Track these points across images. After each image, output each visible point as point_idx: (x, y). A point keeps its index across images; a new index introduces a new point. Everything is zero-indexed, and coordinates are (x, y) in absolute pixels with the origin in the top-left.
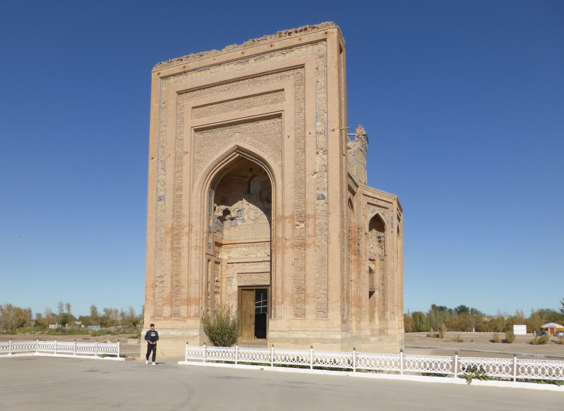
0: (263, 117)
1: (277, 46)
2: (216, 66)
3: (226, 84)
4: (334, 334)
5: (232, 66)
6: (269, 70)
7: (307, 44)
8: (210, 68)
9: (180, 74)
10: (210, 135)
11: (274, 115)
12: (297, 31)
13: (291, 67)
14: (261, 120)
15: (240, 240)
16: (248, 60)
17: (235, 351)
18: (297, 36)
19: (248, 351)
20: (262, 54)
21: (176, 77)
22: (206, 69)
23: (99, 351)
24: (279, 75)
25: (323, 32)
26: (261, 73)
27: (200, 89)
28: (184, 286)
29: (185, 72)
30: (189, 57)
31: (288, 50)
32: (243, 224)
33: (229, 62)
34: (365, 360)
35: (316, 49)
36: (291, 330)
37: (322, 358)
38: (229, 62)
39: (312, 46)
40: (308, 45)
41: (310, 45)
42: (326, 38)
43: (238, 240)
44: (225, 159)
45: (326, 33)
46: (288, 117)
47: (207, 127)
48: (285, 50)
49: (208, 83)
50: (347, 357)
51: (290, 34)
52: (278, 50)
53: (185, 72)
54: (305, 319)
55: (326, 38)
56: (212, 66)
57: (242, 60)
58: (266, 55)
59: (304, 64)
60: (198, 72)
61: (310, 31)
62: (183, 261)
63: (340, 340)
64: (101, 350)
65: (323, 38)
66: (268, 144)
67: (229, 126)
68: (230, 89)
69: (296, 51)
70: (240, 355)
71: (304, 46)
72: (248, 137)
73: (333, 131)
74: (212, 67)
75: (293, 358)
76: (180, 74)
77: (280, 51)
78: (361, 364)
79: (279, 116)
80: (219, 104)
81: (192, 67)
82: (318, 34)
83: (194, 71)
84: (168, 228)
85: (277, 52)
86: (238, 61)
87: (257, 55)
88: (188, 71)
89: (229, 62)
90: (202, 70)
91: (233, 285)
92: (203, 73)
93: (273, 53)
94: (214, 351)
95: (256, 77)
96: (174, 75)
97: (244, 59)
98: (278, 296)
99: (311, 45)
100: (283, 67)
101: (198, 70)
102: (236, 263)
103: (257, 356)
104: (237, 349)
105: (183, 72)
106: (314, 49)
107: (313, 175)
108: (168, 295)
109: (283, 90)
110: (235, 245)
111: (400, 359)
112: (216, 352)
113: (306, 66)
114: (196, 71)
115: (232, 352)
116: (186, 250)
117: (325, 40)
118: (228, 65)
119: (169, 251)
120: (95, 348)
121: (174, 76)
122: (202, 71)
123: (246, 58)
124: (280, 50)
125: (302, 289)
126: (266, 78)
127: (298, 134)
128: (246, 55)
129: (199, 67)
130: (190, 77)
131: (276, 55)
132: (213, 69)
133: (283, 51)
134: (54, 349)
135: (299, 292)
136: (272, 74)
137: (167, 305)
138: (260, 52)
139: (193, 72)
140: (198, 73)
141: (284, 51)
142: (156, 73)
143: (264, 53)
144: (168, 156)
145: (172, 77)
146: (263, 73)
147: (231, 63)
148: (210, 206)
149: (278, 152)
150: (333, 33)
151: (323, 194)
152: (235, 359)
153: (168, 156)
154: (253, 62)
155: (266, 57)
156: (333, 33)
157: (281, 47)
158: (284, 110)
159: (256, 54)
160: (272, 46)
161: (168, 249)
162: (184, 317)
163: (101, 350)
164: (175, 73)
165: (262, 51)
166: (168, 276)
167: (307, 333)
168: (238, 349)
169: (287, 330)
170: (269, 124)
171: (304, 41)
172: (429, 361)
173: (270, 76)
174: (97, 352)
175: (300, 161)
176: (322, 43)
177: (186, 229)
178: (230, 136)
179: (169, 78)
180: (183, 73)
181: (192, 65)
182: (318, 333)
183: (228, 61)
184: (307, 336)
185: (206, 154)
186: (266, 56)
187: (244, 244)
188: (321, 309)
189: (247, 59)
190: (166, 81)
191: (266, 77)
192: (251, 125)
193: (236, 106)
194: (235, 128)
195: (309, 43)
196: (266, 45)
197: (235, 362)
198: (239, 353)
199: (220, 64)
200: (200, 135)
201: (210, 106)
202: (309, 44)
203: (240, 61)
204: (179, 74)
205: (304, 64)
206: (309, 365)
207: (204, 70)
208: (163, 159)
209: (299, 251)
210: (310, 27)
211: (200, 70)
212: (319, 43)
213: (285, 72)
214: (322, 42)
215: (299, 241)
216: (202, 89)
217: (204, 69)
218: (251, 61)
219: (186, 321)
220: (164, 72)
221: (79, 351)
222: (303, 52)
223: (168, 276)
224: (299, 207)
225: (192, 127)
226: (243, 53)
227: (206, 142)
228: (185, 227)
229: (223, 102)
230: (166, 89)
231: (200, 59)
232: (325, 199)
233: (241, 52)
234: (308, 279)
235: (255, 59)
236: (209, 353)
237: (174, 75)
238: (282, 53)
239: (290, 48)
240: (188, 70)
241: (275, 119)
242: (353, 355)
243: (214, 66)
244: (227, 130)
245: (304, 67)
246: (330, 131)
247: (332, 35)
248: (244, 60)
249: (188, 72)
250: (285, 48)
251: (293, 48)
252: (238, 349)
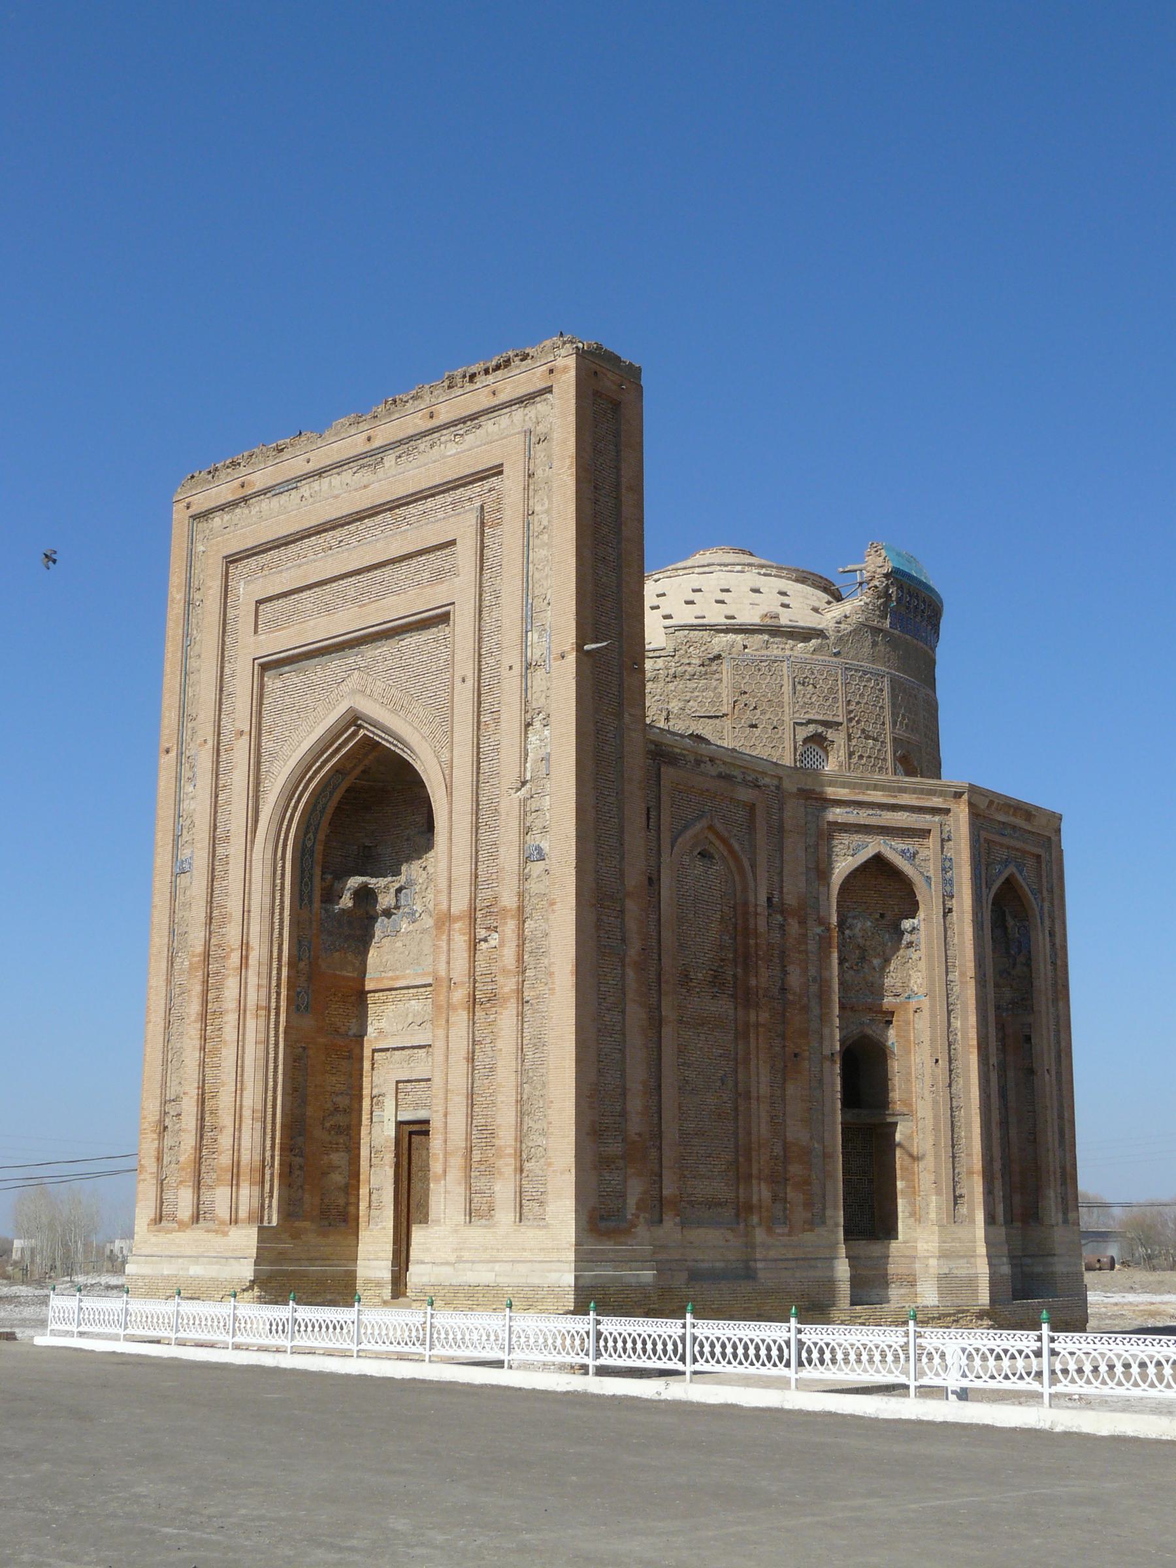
0: (410, 624)
1: (445, 414)
2: (312, 479)
3: (333, 528)
4: (559, 1271)
5: (347, 476)
6: (424, 487)
7: (511, 406)
8: (299, 484)
9: (233, 505)
10: (296, 680)
11: (351, 640)
12: (488, 368)
13: (472, 475)
14: (407, 631)
15: (404, 977)
16: (382, 459)
17: (684, 1334)
18: (488, 383)
19: (732, 1331)
20: (411, 438)
21: (228, 512)
22: (290, 487)
23: (606, 1350)
24: (448, 498)
25: (544, 368)
26: (407, 496)
27: (278, 547)
28: (224, 1127)
29: (245, 499)
30: (254, 456)
31: (469, 423)
32: (411, 928)
33: (341, 466)
34: (1159, 1364)
35: (530, 418)
36: (460, 1260)
37: (1097, 1360)
38: (339, 466)
39: (522, 409)
40: (514, 408)
41: (518, 406)
42: (552, 386)
43: (397, 978)
44: (331, 746)
45: (551, 371)
46: (463, 619)
47: (288, 658)
48: (462, 425)
49: (292, 531)
50: (1170, 1358)
51: (472, 377)
52: (446, 426)
53: (245, 499)
54: (493, 1226)
55: (552, 386)
56: (305, 479)
57: (368, 459)
58: (419, 441)
59: (502, 464)
60: (273, 496)
61: (517, 367)
62: (224, 1052)
63: (569, 1289)
64: (655, 1353)
65: (543, 385)
66: (423, 700)
67: (337, 651)
68: (342, 544)
69: (489, 427)
70: (804, 1355)
71: (505, 411)
72: (378, 683)
73: (563, 657)
74: (303, 482)
75: (1076, 1367)
76: (233, 505)
77: (452, 429)
78: (1114, 1378)
79: (444, 618)
80: (316, 589)
81: (259, 486)
82: (534, 374)
83: (265, 494)
84: (194, 956)
85: (445, 432)
86: (361, 462)
87: (400, 442)
88: (250, 495)
89: (339, 466)
90: (282, 490)
91: (386, 1120)
92: (284, 498)
93: (436, 435)
94: (991, 1351)
95: (398, 507)
96: (221, 508)
97: (371, 458)
98: (435, 1154)
99: (520, 407)
100: (456, 477)
101: (273, 493)
102: (394, 1049)
103: (1148, 1371)
104: (1045, 1339)
105: (241, 498)
106: (527, 418)
107: (520, 789)
108: (189, 1156)
109: (452, 543)
110: (393, 992)
111: (1041, 1348)
112: (974, 1353)
113: (506, 469)
114: (269, 495)
115: (895, 1346)
116: (231, 1018)
117: (549, 390)
118: (338, 474)
119: (195, 1022)
120: (788, 1346)
121: (223, 510)
122: (282, 493)
123: (377, 452)
124: (453, 426)
125: (490, 1132)
126: (421, 508)
127: (489, 669)
128: (376, 443)
129: (274, 483)
130: (257, 512)
131: (443, 439)
132: (305, 489)
133: (459, 427)
134: (588, 1350)
135: (483, 1140)
136: (433, 495)
137: (185, 1186)
138: (406, 436)
139: (262, 497)
140: (275, 499)
141: (460, 428)
142: (184, 504)
143: (418, 437)
144: (200, 745)
145: (218, 513)
146: (412, 495)
147: (346, 467)
148: (306, 884)
149: (443, 724)
150: (565, 369)
151: (541, 845)
152: (684, 1363)
153: (200, 745)
154: (394, 462)
155: (422, 447)
156: (565, 369)
157: (453, 416)
158: (454, 603)
159: (400, 441)
160: (431, 417)
161: (193, 1018)
162: (222, 1223)
163: (625, 1350)
164: (224, 501)
165: (411, 432)
166: (191, 1098)
167: (497, 1267)
168: (1052, 1340)
169: (452, 1259)
170: (426, 643)
171: (503, 397)
172: (993, 1350)
173: (430, 503)
174: (695, 1360)
175: (492, 748)
176: (545, 400)
177: (235, 958)
178: (340, 681)
179: (211, 516)
180: (240, 503)
181: (260, 478)
182: (522, 1268)
183: (338, 465)
184: (496, 1275)
185: (287, 733)
186: (423, 445)
187: (415, 990)
188: (534, 1194)
189: (380, 455)
190: (205, 524)
191: (420, 507)
192: (384, 649)
193: (352, 592)
194: (352, 658)
195: (513, 402)
196: (420, 414)
197: (907, 1387)
198: (801, 1344)
199: (320, 473)
200: (275, 679)
201: (296, 596)
202: (515, 404)
203: (366, 460)
204: (233, 505)
205: (502, 464)
206: (788, 1376)
207: (287, 491)
208: (193, 752)
209: (486, 1017)
210: (517, 355)
211: (277, 491)
212: (538, 399)
213: (463, 489)
214: (544, 396)
215: (485, 988)
216: (282, 545)
217: (286, 488)
218: (390, 459)
219: (228, 1232)
220: (203, 499)
221: (611, 1356)
222: (501, 427)
223: (191, 1098)
224: (487, 886)
225: (254, 659)
226: (369, 439)
227: (288, 700)
228: (232, 950)
229: (326, 584)
230: (204, 549)
231: (277, 461)
232: (544, 859)
233: (364, 435)
234: (502, 1102)
235: (397, 454)
236: (931, 1359)
237: (221, 508)
238: (457, 435)
239: (473, 417)
240: (250, 492)
241: (440, 626)
242: (908, 1337)
243: (308, 480)
244: (336, 664)
245: (501, 473)
246: (555, 659)
247: (565, 377)
248: (374, 458)
249: (251, 498)
250: (463, 421)
251: (480, 418)
252: (1052, 1340)
